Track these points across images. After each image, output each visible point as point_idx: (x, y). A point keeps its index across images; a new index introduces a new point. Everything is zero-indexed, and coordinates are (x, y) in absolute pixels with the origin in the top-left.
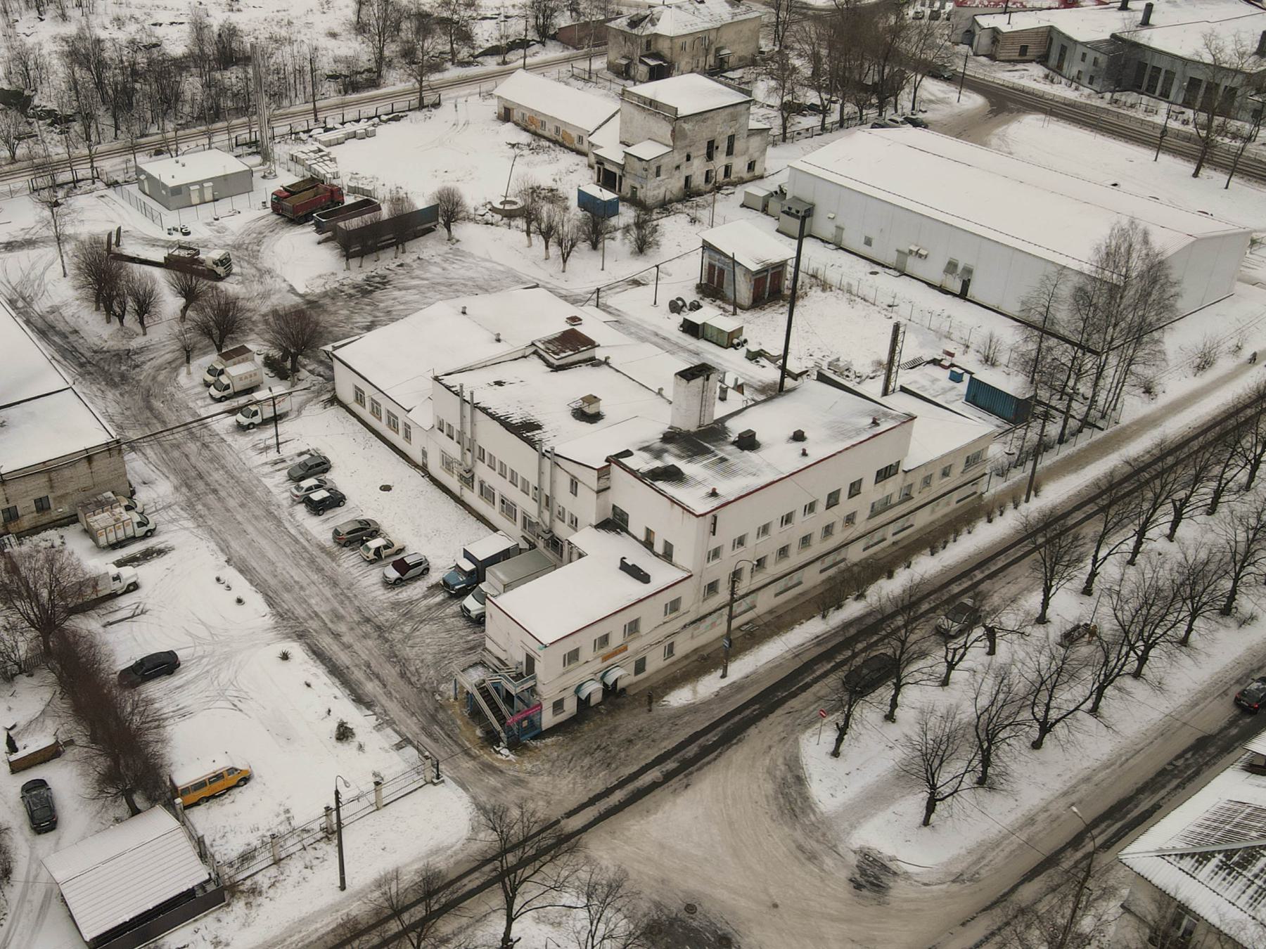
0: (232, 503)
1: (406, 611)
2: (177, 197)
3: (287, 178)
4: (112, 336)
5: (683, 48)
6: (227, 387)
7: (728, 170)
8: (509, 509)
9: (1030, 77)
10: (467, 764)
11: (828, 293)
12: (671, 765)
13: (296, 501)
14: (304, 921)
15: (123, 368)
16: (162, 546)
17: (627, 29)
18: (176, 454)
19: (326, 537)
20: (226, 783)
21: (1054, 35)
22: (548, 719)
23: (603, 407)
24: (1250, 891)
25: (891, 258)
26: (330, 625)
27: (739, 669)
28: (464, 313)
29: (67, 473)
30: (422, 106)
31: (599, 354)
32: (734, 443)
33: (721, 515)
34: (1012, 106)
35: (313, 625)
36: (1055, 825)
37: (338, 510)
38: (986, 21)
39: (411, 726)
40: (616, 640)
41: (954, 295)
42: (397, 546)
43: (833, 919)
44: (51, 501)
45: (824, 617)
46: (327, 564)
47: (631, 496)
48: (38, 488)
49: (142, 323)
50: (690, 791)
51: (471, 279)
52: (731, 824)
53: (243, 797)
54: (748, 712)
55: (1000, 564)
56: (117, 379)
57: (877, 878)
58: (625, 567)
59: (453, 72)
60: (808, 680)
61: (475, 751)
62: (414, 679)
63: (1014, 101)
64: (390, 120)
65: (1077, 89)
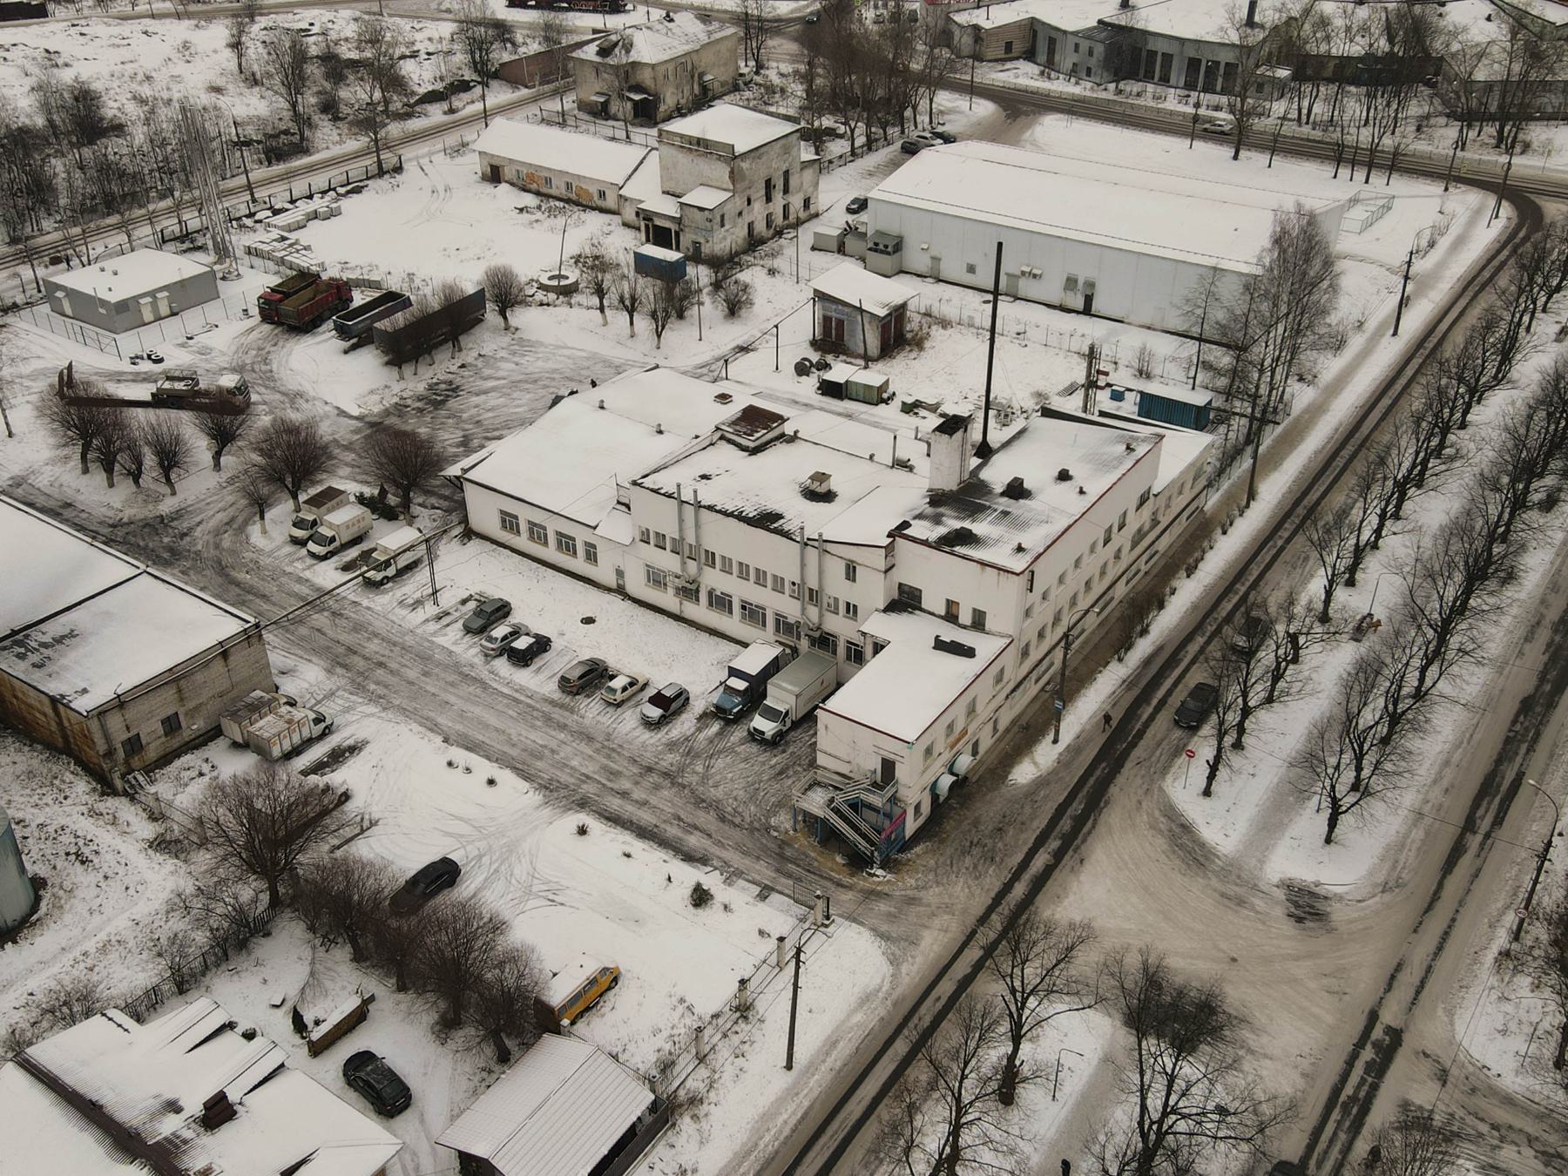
0: (412, 674)
2: (124, 315)
4: (128, 502)
5: (666, 77)
6: (333, 539)
8: (753, 614)
9: (1023, 75)
10: (847, 896)
11: (950, 331)
12: (1054, 844)
13: (488, 656)
14: (767, 1117)
15: (166, 540)
16: (351, 742)
17: (598, 59)
19: (550, 688)
20: (604, 984)
22: (911, 826)
23: (834, 484)
26: (609, 784)
28: (602, 408)
30: (381, 173)
31: (788, 429)
32: (1003, 494)
35: (589, 789)
37: (547, 656)
41: (1078, 312)
42: (641, 681)
43: (1297, 959)
44: (182, 718)
45: (1120, 660)
46: (571, 719)
48: (165, 704)
49: (168, 481)
51: (555, 371)
52: (1146, 889)
53: (621, 1001)
54: (1098, 773)
55: (1256, 573)
56: (166, 555)
57: (1312, 907)
58: (940, 645)
60: (1138, 726)
61: (847, 880)
62: (737, 820)
63: (1023, 103)
64: (348, 192)
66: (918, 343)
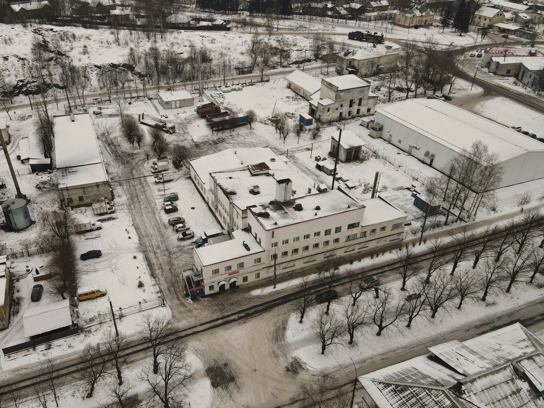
1: (181, 249)
2: (167, 105)
3: (206, 102)
6: (156, 169)
7: (358, 111)
9: (508, 83)
10: (176, 302)
11: (377, 159)
12: (242, 315)
18: (133, 188)
21: (522, 67)
23: (260, 189)
24: (400, 402)
25: (407, 148)
27: (280, 287)
29: (90, 189)
30: (262, 81)
31: (271, 172)
32: (294, 208)
33: (275, 231)
34: (493, 93)
36: (373, 365)
38: (495, 59)
39: (164, 286)
40: (234, 268)
41: (427, 164)
42: (187, 227)
43: (274, 380)
47: (252, 220)
48: (80, 193)
50: (244, 325)
52: (253, 339)
55: (397, 266)
57: (296, 369)
59: (280, 69)
62: (173, 271)
63: (496, 91)
65: (525, 88)
66: (362, 160)
